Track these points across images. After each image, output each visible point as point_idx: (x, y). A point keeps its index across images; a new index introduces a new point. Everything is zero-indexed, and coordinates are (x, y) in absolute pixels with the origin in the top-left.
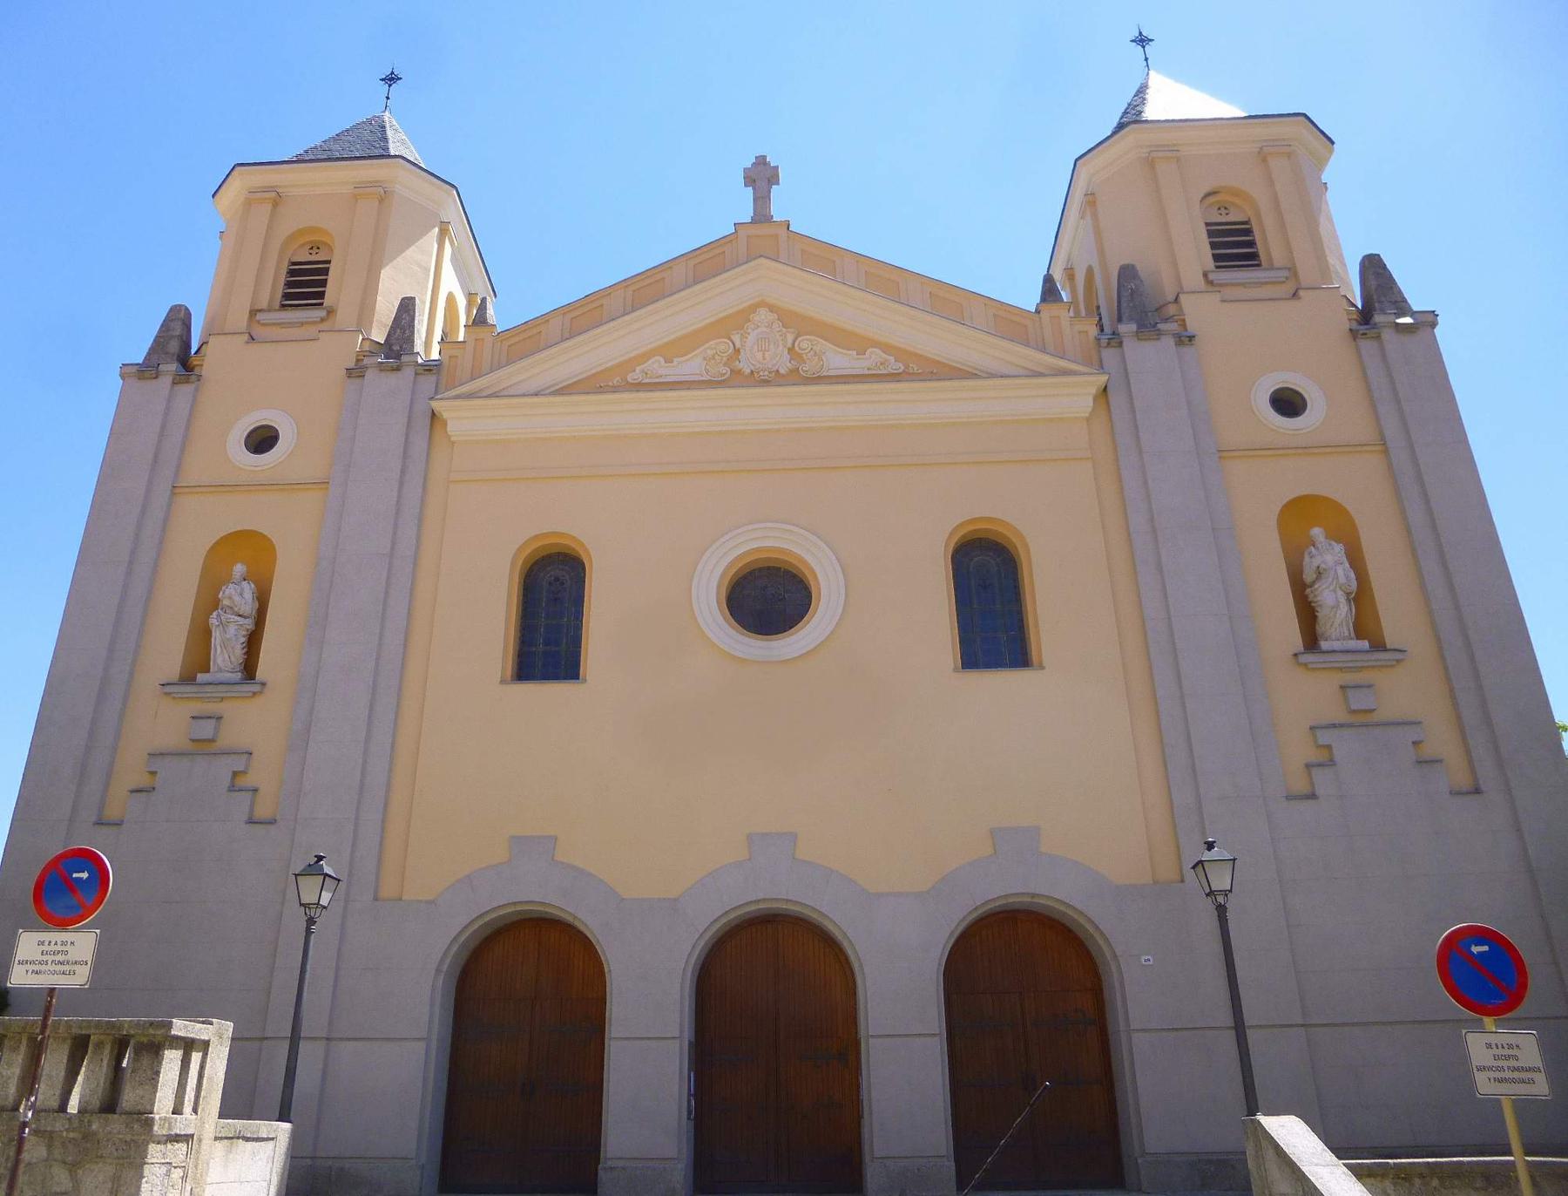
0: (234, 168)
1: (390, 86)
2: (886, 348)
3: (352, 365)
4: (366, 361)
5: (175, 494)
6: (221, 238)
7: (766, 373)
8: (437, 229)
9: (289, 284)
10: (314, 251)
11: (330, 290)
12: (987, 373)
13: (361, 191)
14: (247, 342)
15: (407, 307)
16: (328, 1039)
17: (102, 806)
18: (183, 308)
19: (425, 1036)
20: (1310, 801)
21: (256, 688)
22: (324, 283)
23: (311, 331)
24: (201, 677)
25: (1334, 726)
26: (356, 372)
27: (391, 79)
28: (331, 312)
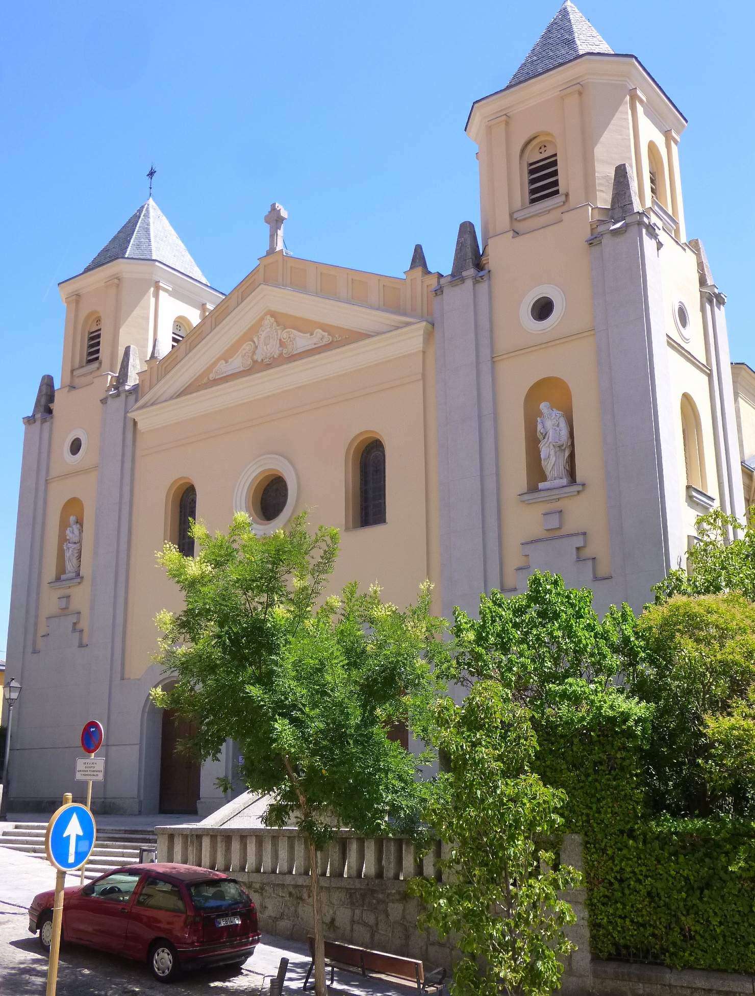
2: (324, 328)
3: (588, 235)
4: (601, 229)
7: (268, 359)
8: (628, 97)
9: (532, 182)
11: (561, 178)
13: (493, 122)
15: (621, 173)
16: (108, 746)
18: (468, 224)
21: (79, 580)
23: (555, 215)
24: (541, 485)
25: (536, 541)
26: (594, 241)
28: (567, 195)
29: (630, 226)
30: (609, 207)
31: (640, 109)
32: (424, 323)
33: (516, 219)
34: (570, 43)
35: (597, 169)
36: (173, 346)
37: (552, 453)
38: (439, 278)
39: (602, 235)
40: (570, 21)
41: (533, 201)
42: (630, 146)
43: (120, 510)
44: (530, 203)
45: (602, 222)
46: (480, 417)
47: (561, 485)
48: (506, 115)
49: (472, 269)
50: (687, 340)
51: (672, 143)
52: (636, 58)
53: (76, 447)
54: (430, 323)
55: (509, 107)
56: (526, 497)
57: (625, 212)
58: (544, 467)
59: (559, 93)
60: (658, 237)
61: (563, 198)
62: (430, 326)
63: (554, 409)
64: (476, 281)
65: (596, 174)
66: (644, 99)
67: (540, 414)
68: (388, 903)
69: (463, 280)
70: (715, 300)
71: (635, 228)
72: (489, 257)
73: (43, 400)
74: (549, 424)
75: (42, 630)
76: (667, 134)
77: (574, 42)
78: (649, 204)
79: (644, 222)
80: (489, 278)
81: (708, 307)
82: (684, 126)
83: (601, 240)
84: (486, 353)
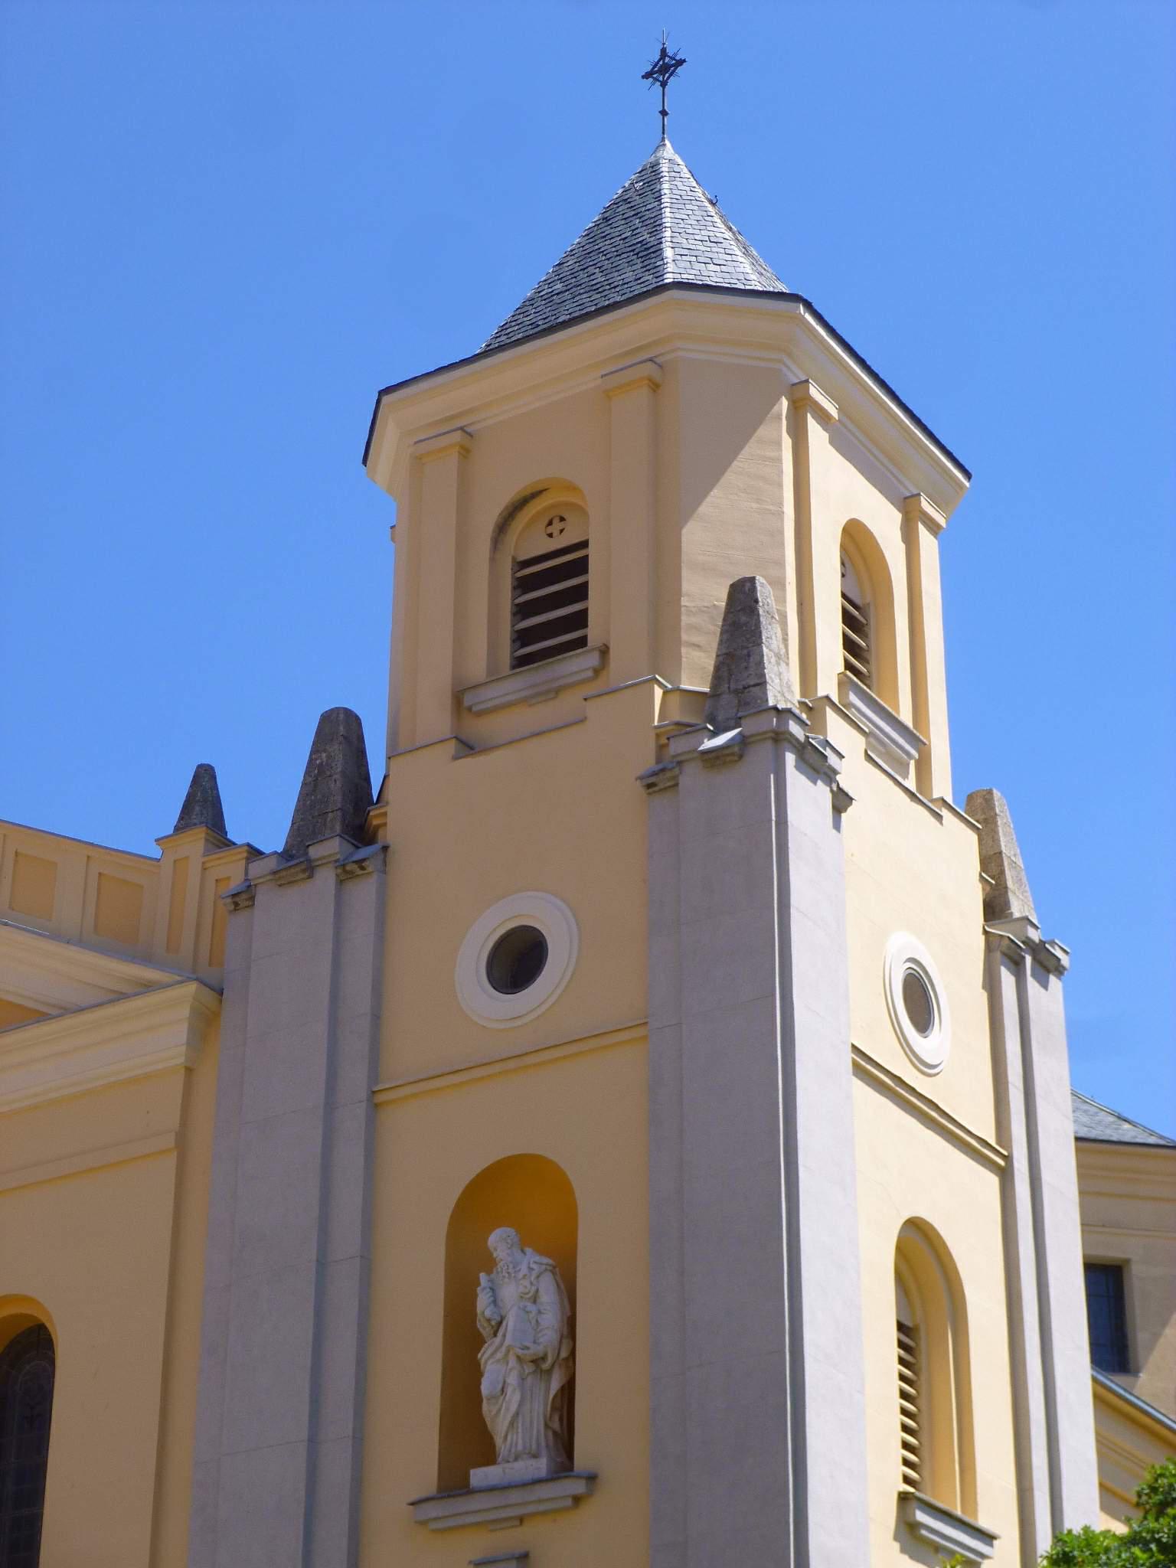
0: (378, 402)
1: (664, 84)
3: (649, 763)
5: (376, 1105)
8: (784, 403)
9: (522, 611)
11: (594, 604)
12: (61, 1008)
14: (456, 758)
18: (342, 716)
21: (578, 1487)
24: (479, 1476)
27: (665, 68)
28: (604, 651)
29: (750, 743)
30: (707, 690)
31: (817, 435)
32: (193, 987)
33: (470, 709)
34: (651, 253)
35: (685, 586)
37: (513, 1380)
38: (249, 860)
39: (680, 763)
40: (659, 199)
41: (521, 662)
42: (781, 532)
44: (513, 667)
45: (685, 729)
46: (322, 1265)
47: (528, 1476)
48: (462, 429)
49: (337, 840)
50: (935, 1067)
51: (921, 528)
52: (808, 306)
54: (212, 989)
55: (471, 411)
56: (432, 1510)
57: (747, 704)
58: (488, 1420)
59: (599, 381)
60: (838, 777)
61: (593, 659)
62: (209, 997)
63: (528, 1250)
64: (347, 873)
65: (684, 601)
66: (832, 410)
67: (489, 1263)
69: (310, 869)
70: (1028, 959)
71: (763, 752)
72: (388, 809)
74: (509, 1292)
76: (908, 507)
77: (658, 252)
78: (827, 684)
79: (792, 735)
80: (384, 869)
81: (1007, 979)
82: (961, 486)
83: (675, 778)
84: (354, 1079)
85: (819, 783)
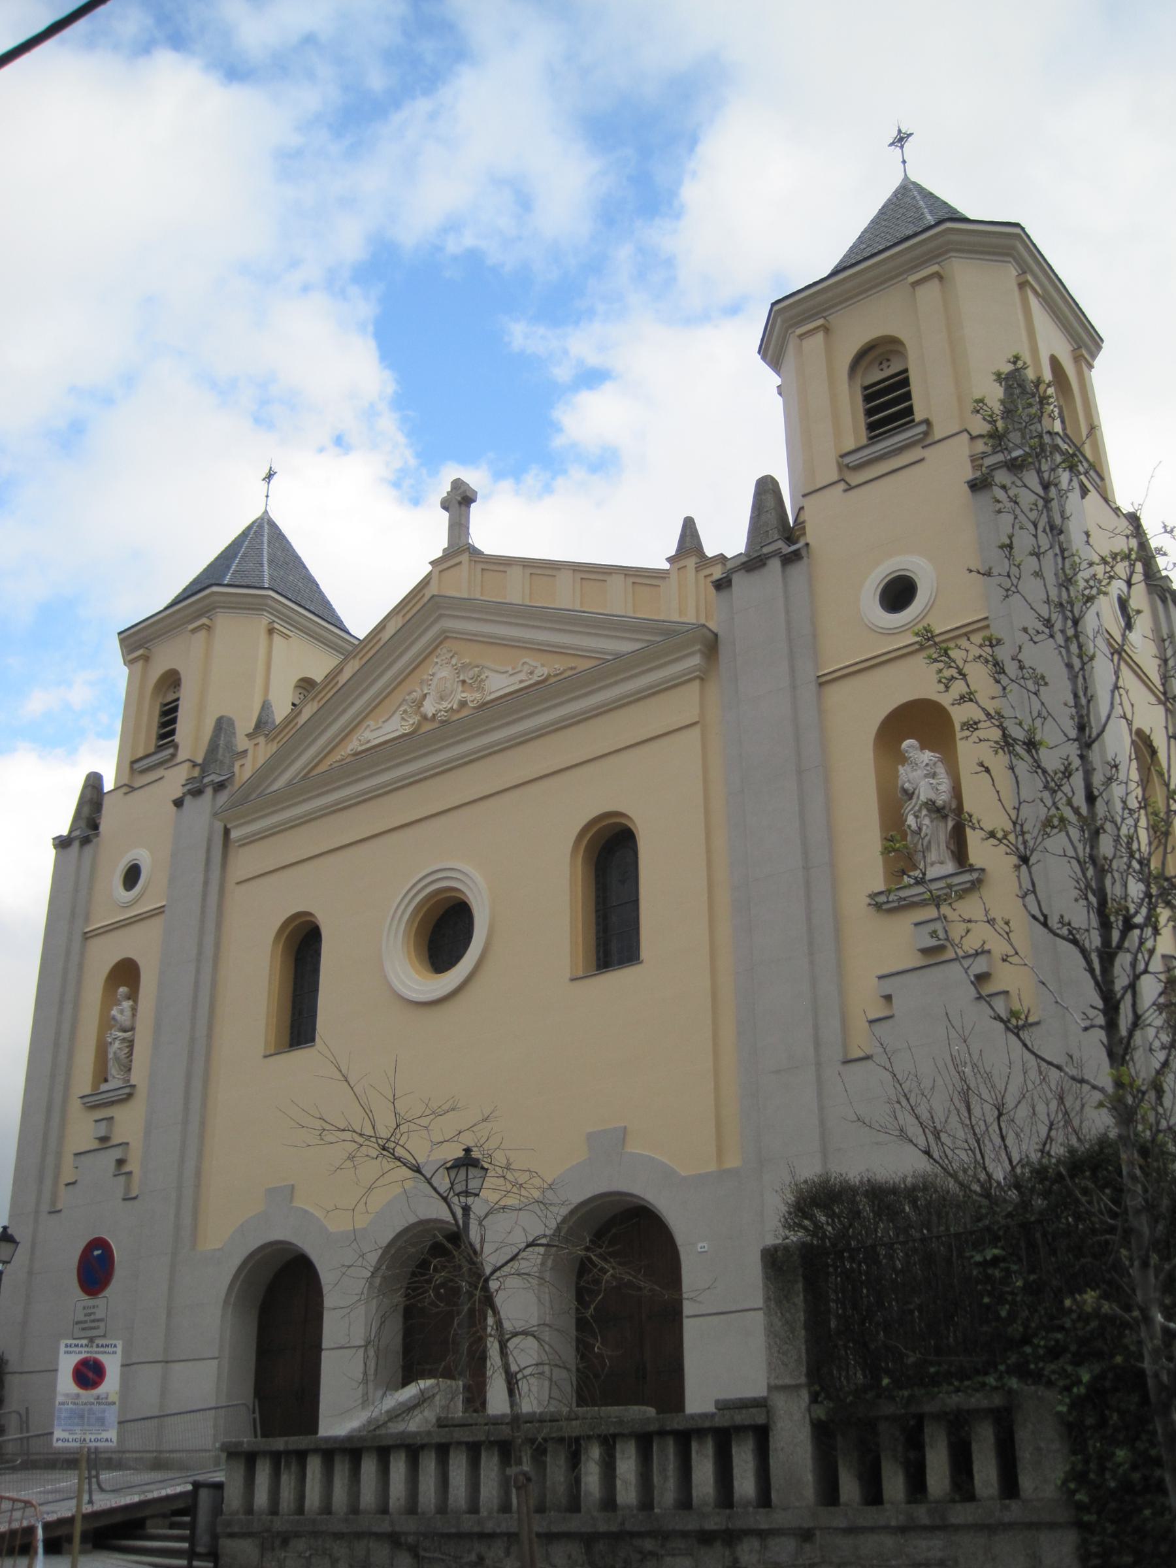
1: (902, 147)
6: (780, 394)
9: (869, 413)
10: (884, 365)
17: (845, 1046)
19: (217, 1355)
20: (969, 934)
22: (908, 396)
36: (292, 709)
43: (198, 972)
53: (132, 876)
68: (662, 1556)
73: (86, 810)
75: (67, 1175)
85: (711, 1408)
